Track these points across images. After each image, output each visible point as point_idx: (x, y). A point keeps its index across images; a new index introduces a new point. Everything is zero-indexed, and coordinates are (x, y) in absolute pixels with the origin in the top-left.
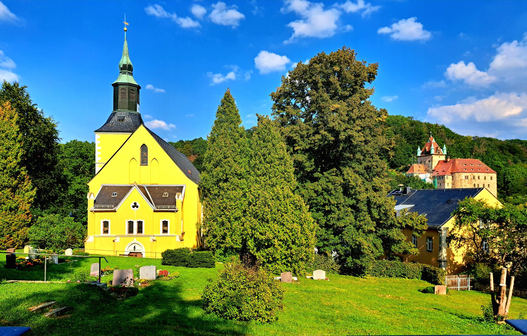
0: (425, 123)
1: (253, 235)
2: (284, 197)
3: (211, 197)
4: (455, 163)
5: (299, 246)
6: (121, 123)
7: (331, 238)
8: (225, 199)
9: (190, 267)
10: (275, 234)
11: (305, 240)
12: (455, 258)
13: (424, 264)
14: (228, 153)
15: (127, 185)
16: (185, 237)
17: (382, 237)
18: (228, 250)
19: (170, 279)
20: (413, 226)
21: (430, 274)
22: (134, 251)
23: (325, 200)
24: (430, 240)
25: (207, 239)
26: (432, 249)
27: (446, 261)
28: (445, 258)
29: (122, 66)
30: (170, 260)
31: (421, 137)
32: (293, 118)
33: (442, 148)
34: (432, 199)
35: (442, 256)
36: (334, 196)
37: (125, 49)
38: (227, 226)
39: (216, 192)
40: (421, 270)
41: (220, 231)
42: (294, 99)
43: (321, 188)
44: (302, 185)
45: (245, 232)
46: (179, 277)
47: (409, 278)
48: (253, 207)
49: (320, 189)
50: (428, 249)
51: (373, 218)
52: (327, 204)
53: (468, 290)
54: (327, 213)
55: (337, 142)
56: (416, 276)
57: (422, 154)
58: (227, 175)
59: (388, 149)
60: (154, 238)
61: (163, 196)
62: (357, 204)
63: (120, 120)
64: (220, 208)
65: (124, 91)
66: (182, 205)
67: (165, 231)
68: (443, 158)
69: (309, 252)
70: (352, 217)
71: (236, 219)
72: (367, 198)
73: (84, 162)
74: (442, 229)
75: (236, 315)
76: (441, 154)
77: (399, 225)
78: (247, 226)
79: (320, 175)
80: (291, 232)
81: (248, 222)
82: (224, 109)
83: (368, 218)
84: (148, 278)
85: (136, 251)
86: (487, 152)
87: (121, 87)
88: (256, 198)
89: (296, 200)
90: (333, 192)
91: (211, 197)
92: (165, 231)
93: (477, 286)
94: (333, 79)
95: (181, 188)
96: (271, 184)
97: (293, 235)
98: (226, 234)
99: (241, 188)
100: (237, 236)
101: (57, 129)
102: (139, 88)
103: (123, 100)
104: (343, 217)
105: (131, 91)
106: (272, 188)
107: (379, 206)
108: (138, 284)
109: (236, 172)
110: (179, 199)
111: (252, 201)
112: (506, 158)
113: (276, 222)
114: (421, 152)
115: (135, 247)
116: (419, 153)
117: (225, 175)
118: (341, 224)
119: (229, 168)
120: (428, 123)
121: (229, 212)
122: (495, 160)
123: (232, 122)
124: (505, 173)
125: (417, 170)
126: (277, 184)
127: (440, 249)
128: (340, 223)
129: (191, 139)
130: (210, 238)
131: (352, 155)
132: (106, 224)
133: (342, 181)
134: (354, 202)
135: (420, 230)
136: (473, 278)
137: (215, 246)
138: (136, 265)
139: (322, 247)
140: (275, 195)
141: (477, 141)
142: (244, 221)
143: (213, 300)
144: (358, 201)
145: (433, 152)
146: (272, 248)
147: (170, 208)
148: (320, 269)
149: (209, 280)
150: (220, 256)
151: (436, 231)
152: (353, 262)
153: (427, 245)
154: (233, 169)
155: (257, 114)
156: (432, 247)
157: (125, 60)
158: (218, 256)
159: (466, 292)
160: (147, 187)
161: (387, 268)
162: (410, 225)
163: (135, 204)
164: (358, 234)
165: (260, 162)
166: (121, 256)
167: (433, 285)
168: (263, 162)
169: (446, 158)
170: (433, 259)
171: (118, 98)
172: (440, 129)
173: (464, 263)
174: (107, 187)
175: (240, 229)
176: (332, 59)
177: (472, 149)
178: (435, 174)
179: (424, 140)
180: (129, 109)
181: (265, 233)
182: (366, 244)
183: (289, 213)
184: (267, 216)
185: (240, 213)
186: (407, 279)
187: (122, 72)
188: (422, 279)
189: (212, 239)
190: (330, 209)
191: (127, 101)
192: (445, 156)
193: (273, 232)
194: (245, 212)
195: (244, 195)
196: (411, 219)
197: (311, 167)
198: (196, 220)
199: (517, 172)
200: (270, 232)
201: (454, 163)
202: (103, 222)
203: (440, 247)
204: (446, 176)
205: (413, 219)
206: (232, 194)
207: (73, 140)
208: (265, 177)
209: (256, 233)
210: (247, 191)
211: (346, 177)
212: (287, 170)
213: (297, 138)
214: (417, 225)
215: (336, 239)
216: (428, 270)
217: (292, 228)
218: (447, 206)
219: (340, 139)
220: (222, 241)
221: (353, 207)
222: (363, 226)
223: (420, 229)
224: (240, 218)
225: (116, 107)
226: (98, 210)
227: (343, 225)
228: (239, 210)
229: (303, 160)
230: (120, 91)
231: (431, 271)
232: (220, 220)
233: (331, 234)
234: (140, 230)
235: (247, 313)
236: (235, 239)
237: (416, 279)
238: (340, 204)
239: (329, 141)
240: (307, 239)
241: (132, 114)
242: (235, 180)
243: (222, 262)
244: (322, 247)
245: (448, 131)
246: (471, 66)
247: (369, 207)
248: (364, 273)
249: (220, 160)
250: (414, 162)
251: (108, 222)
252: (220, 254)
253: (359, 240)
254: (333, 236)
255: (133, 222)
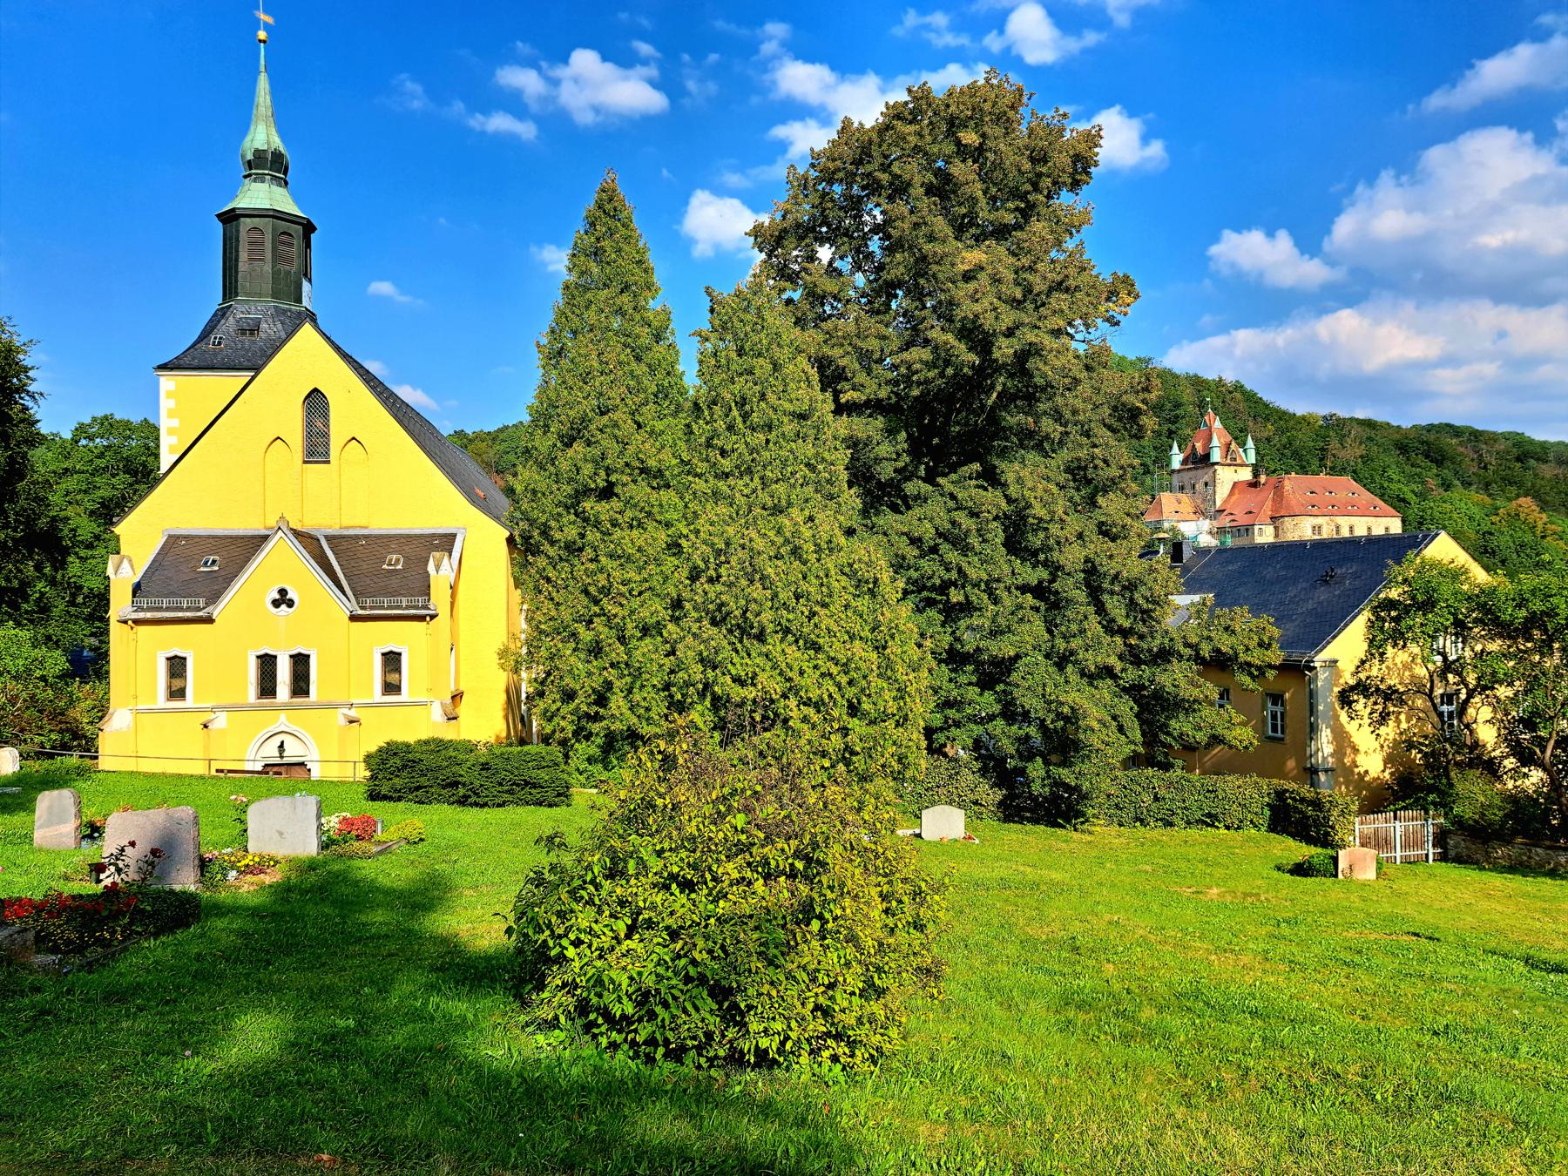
0: (1188, 377)
1: (707, 686)
2: (819, 550)
3: (552, 551)
4: (1283, 487)
5: (872, 722)
6: (247, 339)
7: (969, 697)
8: (603, 559)
9: (476, 804)
10: (790, 680)
11: (894, 699)
12: (1360, 759)
13: (1275, 781)
14: (612, 394)
15: (256, 533)
16: (463, 709)
17: (1134, 690)
18: (617, 745)
19: (380, 853)
20: (1236, 654)
21: (1301, 812)
22: (278, 761)
23: (948, 570)
24: (1275, 703)
25: (541, 705)
26: (1283, 732)
27: (1332, 770)
28: (1330, 759)
29: (250, 156)
30: (396, 780)
31: (1177, 417)
32: (824, 311)
33: (1243, 444)
34: (1269, 573)
35: (1320, 754)
36: (976, 554)
37: (261, 100)
38: (614, 655)
39: (572, 533)
40: (1266, 799)
41: (589, 674)
42: (827, 245)
43: (933, 531)
44: (864, 522)
45: (681, 674)
46: (422, 840)
47: (1228, 828)
48: (706, 586)
49: (927, 531)
50: (1270, 733)
51: (1111, 628)
52: (954, 584)
53: (1427, 861)
54: (952, 613)
55: (988, 367)
56: (1251, 821)
57: (1185, 462)
58: (608, 471)
59: (1141, 405)
60: (353, 713)
61: (385, 566)
62: (1053, 581)
63: (243, 331)
64: (586, 592)
65: (257, 235)
66: (453, 596)
67: (391, 688)
68: (1246, 474)
69: (911, 743)
70: (1038, 626)
71: (645, 631)
72: (1086, 562)
73: (137, 486)
74: (1317, 664)
75: (709, 1036)
76: (1239, 462)
77: (1187, 652)
78: (689, 653)
79: (926, 488)
80: (846, 673)
81: (689, 639)
82: (598, 240)
83: (1094, 626)
84: (281, 850)
85: (285, 760)
86: (1366, 459)
87: (246, 223)
88: (718, 553)
89: (860, 560)
90: (974, 541)
91: (552, 551)
92: (391, 688)
93: (1456, 847)
94: (961, 170)
95: (451, 538)
96: (770, 504)
97: (851, 683)
98: (609, 685)
99: (660, 522)
100: (649, 693)
101: (28, 361)
102: (309, 228)
103: (256, 268)
104: (1008, 627)
105: (283, 237)
106: (772, 518)
107: (1131, 586)
108: (225, 875)
109: (643, 462)
110: (440, 574)
111: (702, 566)
112: (1419, 475)
113: (790, 638)
114: (1181, 457)
115: (282, 745)
116: (1177, 459)
117: (603, 473)
118: (1004, 648)
119: (618, 448)
120: (1196, 376)
121: (621, 605)
122: (1390, 480)
123: (626, 288)
124: (1422, 517)
125: (1173, 510)
126: (790, 504)
127: (1313, 729)
128: (1002, 645)
129: (492, 428)
130: (551, 701)
131: (1030, 419)
132: (177, 666)
133: (1004, 504)
134: (1044, 574)
135: (1259, 668)
136: (1442, 821)
137: (570, 728)
138: (233, 797)
139: (941, 729)
140: (787, 541)
141: (1335, 426)
142: (674, 636)
143: (571, 952)
144: (1056, 569)
145: (1216, 456)
146: (778, 729)
147: (408, 607)
148: (934, 803)
149: (550, 839)
150: (590, 768)
151: (1297, 670)
152: (1049, 777)
153: (1264, 720)
154: (631, 449)
155: (707, 288)
156: (1282, 726)
157: (263, 136)
158: (582, 767)
159: (1420, 869)
160: (326, 537)
161: (1155, 796)
162: (1224, 649)
163: (283, 592)
164: (1062, 680)
165: (730, 428)
166: (222, 775)
167: (1330, 852)
168: (741, 426)
169: (1256, 474)
170: (1291, 764)
171: (237, 260)
172: (1231, 392)
173: (1387, 775)
174: (186, 537)
175: (661, 666)
176: (953, 108)
177: (1322, 449)
178: (1225, 521)
179: (1188, 425)
180: (276, 295)
181: (752, 679)
182: (1094, 715)
183: (836, 607)
184: (758, 614)
185: (659, 608)
186: (1223, 831)
187: (250, 175)
188: (1273, 828)
189: (559, 704)
190: (967, 597)
191: (268, 268)
192: (1250, 469)
193: (781, 674)
194: (677, 604)
195: (674, 547)
196: (1227, 629)
197: (895, 460)
198: (499, 638)
199: (1455, 515)
200: (769, 674)
201: (1278, 489)
202: (168, 659)
203: (1311, 724)
204: (1256, 528)
205: (1233, 632)
206: (629, 539)
207: (100, 414)
208: (747, 479)
209: (721, 680)
210: (685, 532)
211: (1013, 491)
212: (826, 455)
213: (849, 363)
214: (1248, 649)
215: (987, 702)
216: (1294, 799)
217: (848, 660)
218: (1322, 594)
219: (996, 360)
220: (597, 713)
221: (1039, 591)
222: (1081, 652)
223: (1258, 662)
224: (659, 627)
225: (230, 289)
226: (149, 615)
227: (1012, 653)
228: (657, 600)
229: (869, 437)
230: (243, 235)
231: (1303, 800)
232: (586, 636)
233: (970, 684)
234: (302, 684)
235: (778, 1026)
236: (643, 704)
237: (1253, 831)
238: (998, 580)
239: (959, 369)
240: (902, 698)
241: (284, 311)
242: (641, 491)
243: (596, 787)
244: (941, 729)
245: (1251, 398)
246: (1284, 242)
247: (1095, 593)
248: (1083, 814)
249: (584, 419)
250: (1162, 489)
251: (185, 659)
252: (590, 760)
253: (1070, 700)
254: (977, 690)
255: (275, 657)
